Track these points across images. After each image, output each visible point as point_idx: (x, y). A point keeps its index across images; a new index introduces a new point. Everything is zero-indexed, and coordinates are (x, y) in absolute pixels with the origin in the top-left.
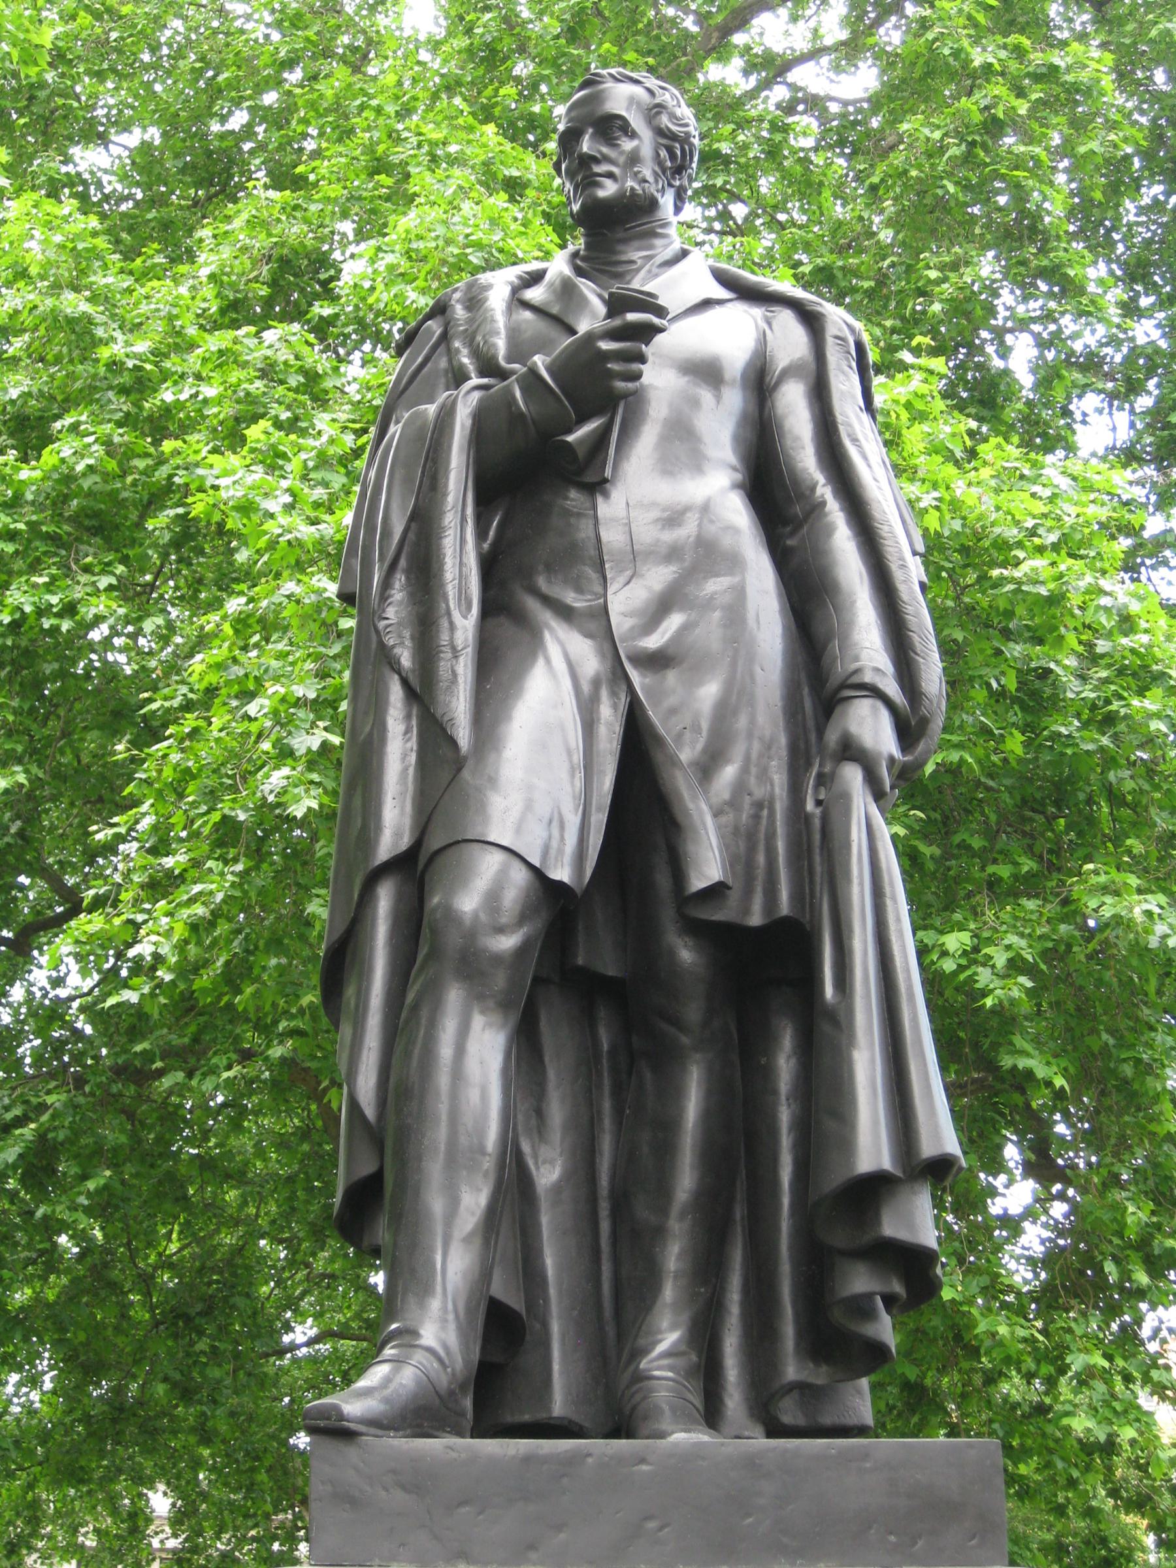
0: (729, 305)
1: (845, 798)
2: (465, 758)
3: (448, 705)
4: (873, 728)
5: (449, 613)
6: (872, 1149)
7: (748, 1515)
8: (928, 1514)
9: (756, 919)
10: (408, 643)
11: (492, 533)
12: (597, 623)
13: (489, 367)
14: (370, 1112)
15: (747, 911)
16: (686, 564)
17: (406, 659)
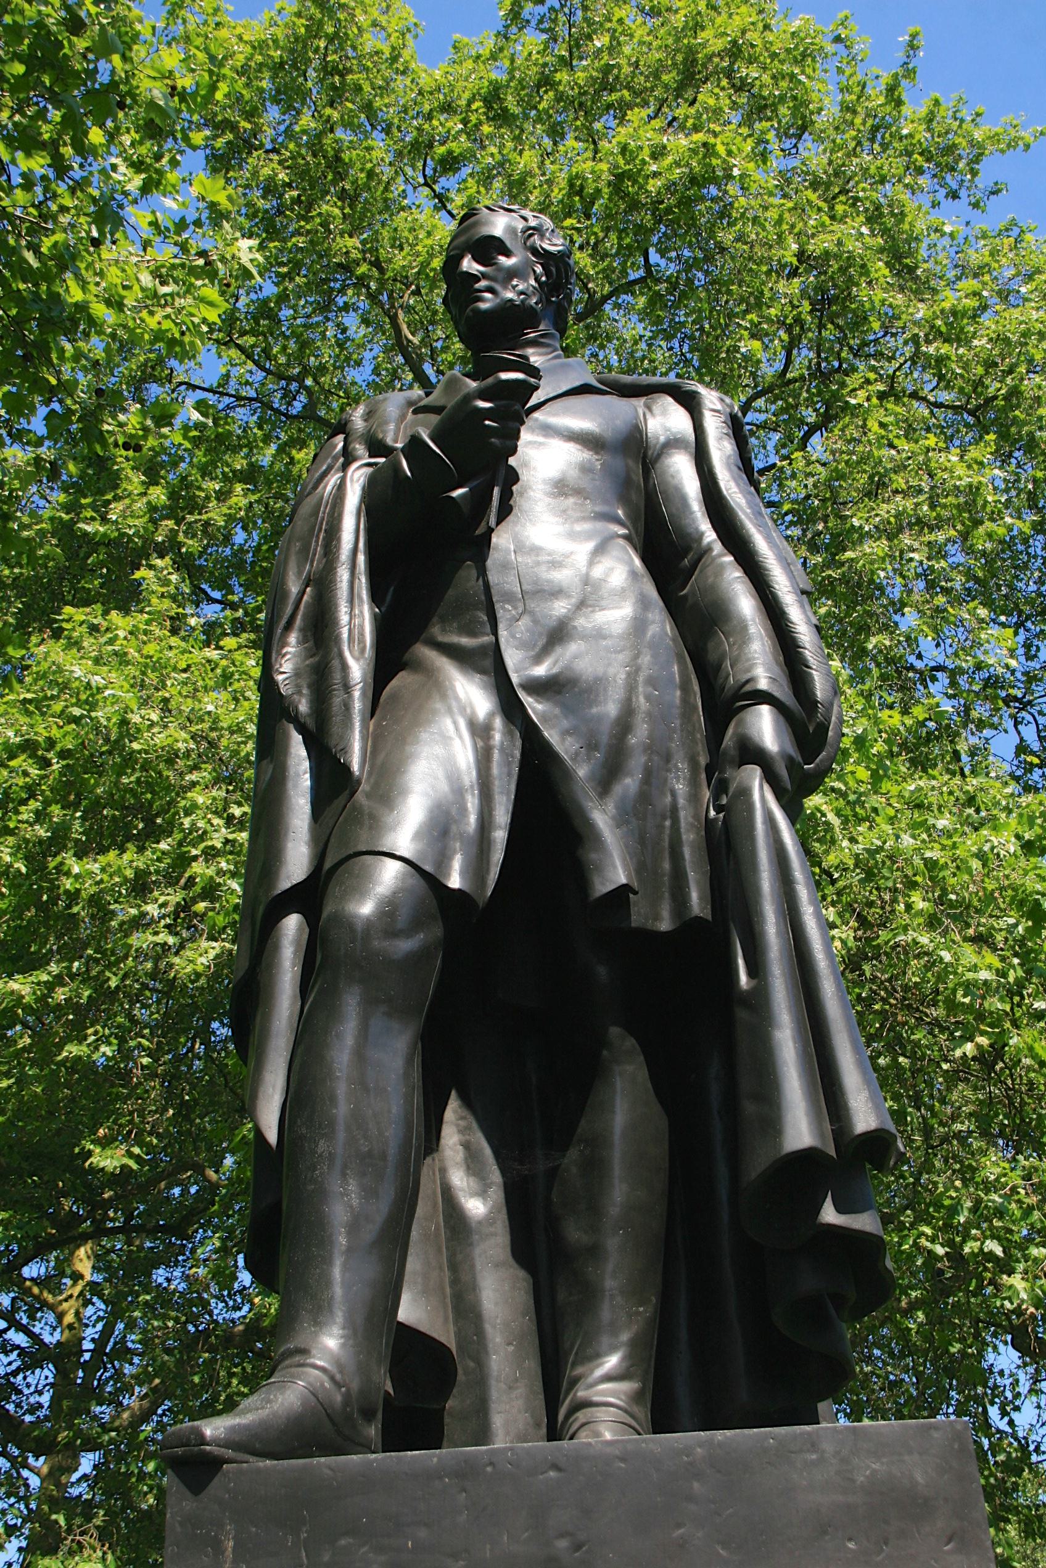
0: (608, 397)
1: (745, 793)
2: (359, 782)
3: (342, 738)
4: (765, 727)
5: (341, 655)
6: (800, 1129)
7: (679, 1526)
8: (894, 1510)
9: (665, 925)
10: (305, 691)
11: (389, 598)
12: (490, 665)
13: (377, 447)
14: (272, 1137)
15: (657, 917)
16: (573, 600)
17: (303, 707)
